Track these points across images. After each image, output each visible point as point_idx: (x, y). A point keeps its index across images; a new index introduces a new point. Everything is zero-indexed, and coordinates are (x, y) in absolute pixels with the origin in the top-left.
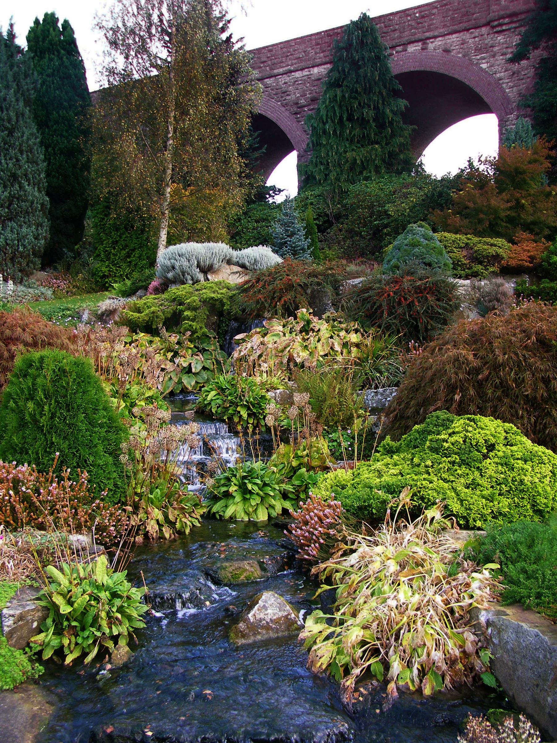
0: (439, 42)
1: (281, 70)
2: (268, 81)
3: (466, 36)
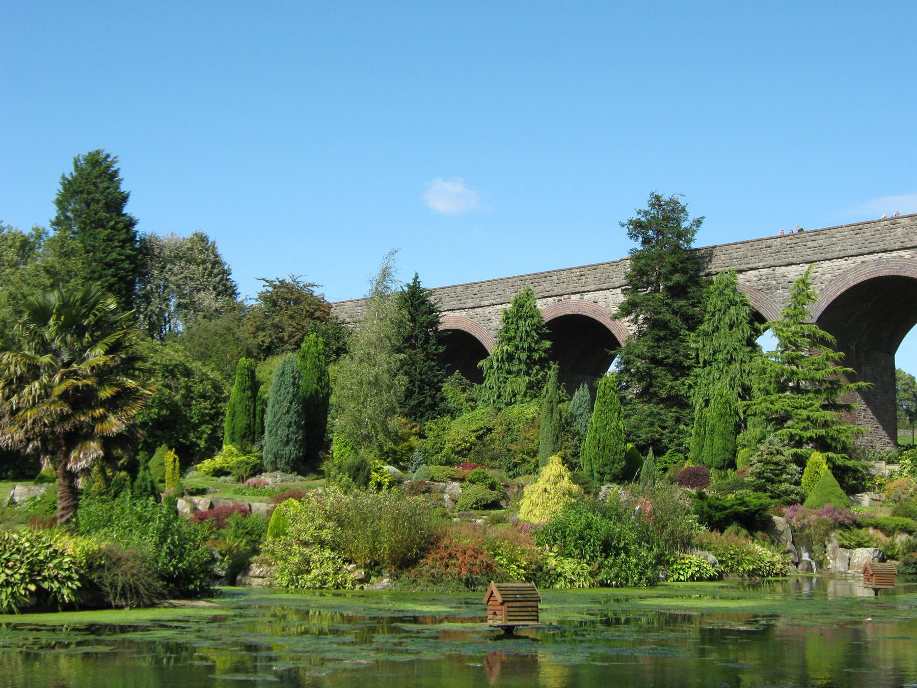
0: (590, 295)
1: (487, 303)
2: (478, 310)
3: (607, 292)
